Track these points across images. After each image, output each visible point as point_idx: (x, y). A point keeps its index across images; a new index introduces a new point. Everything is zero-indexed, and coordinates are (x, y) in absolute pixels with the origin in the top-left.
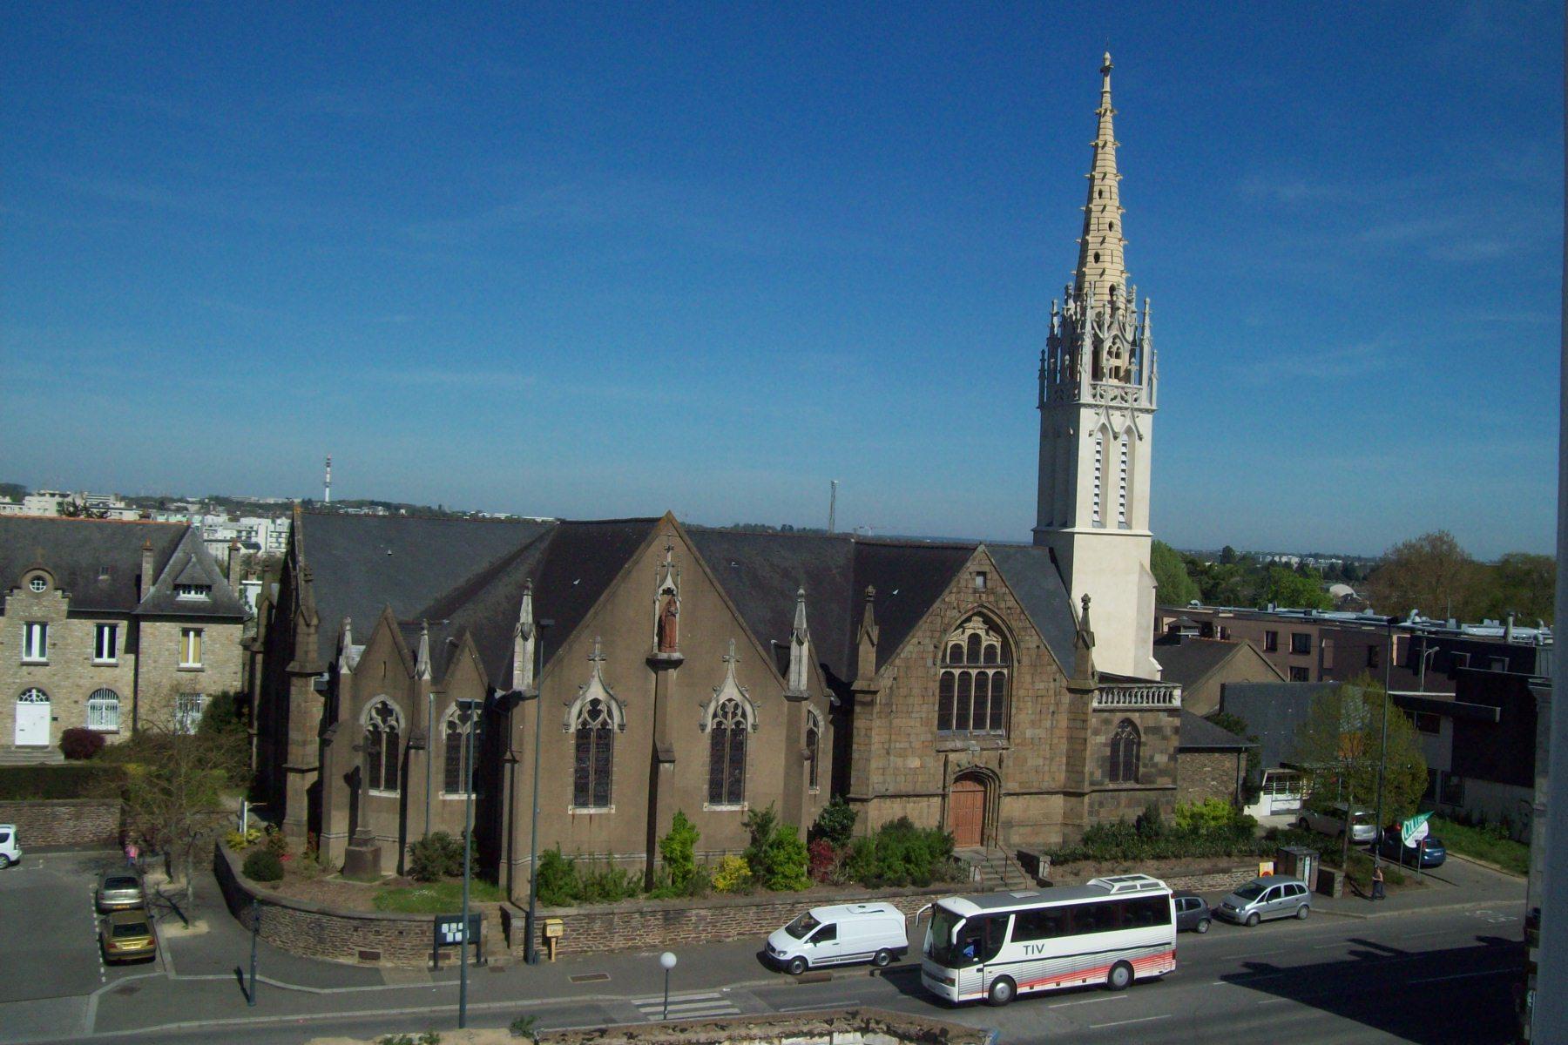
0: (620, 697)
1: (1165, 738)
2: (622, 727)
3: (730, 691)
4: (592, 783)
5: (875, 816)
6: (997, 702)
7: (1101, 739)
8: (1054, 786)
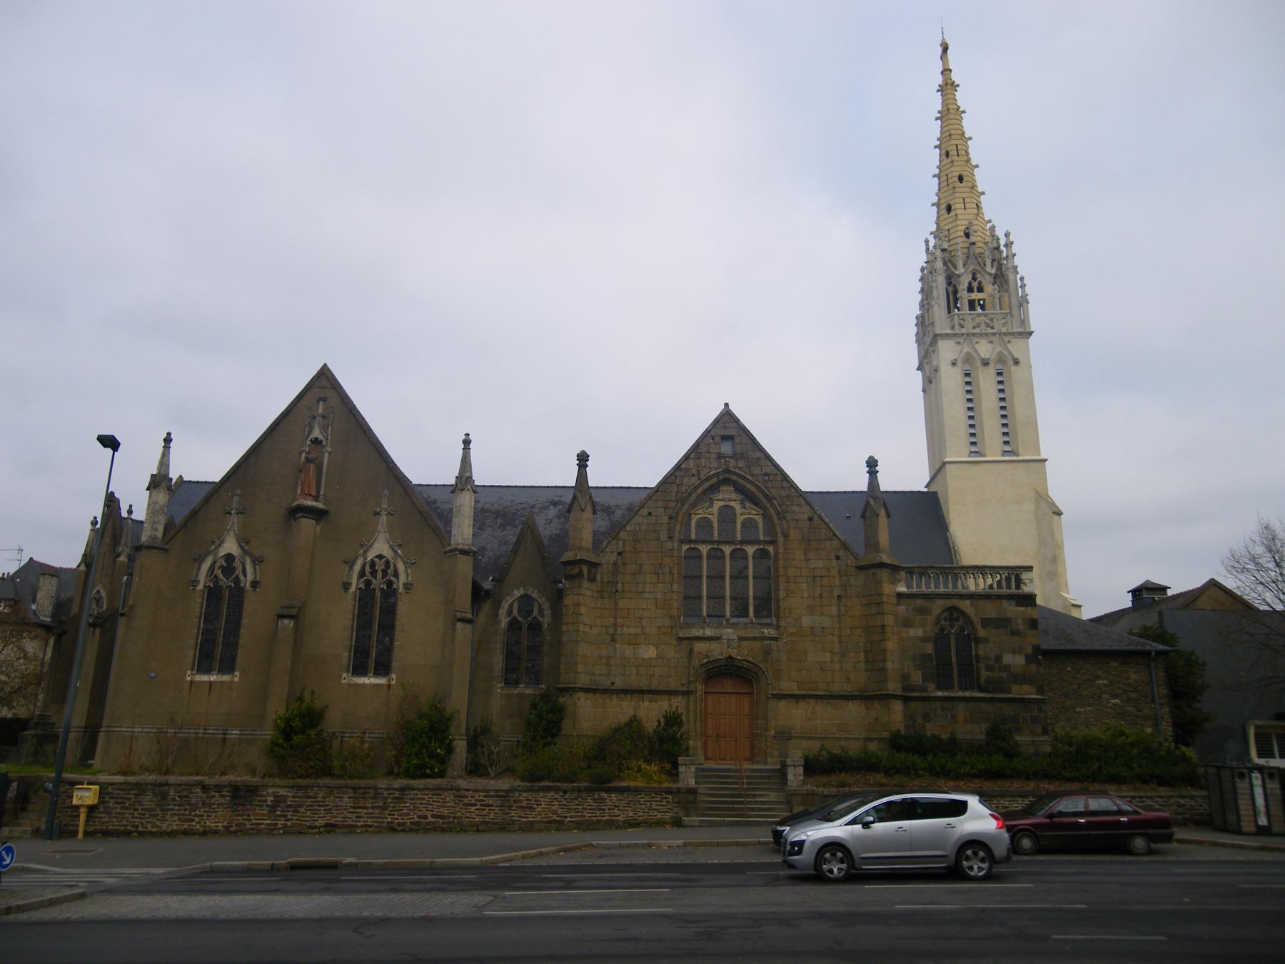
1: (1015, 633)
2: (255, 584)
3: (381, 547)
4: (216, 650)
5: (590, 717)
8: (848, 689)
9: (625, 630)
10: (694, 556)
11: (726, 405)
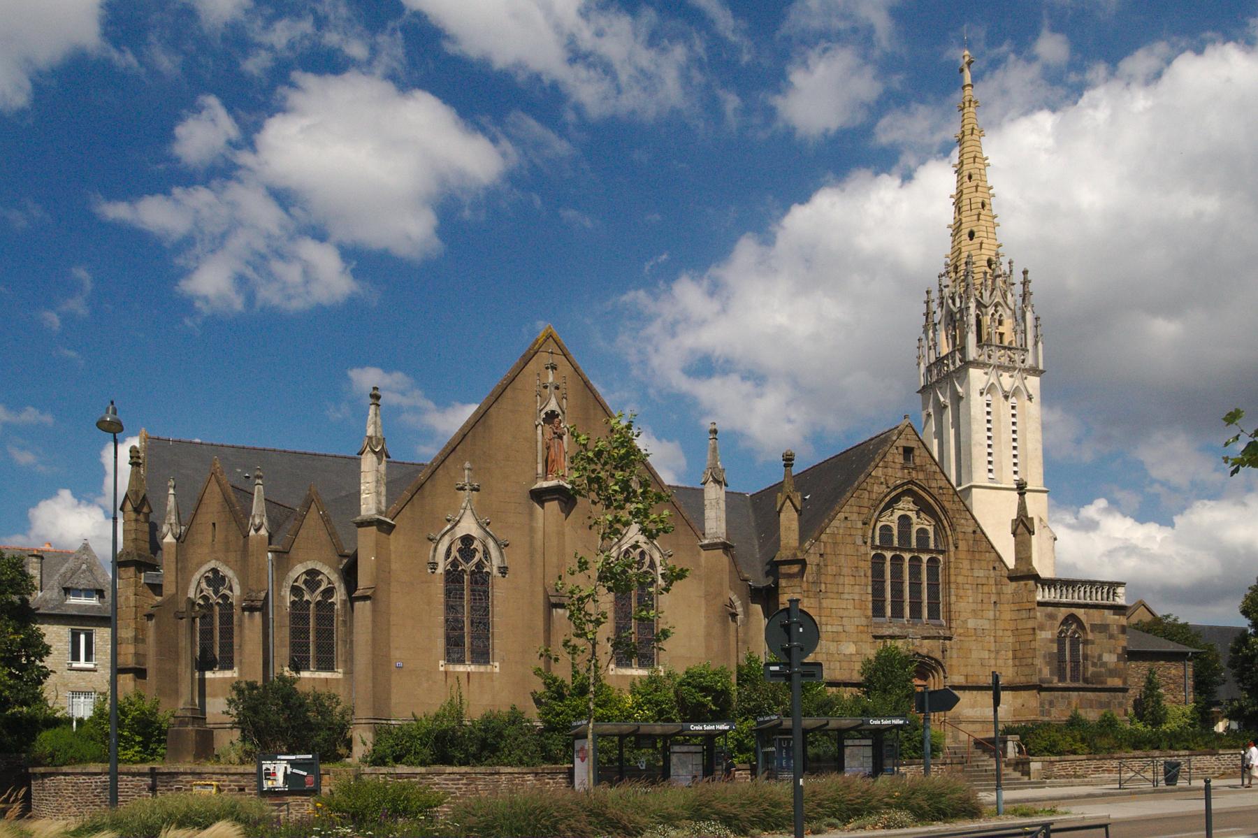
0: (502, 537)
1: (1111, 637)
2: (504, 571)
4: (468, 636)
6: (934, 588)
7: (1046, 635)
9: (829, 628)
10: (879, 559)
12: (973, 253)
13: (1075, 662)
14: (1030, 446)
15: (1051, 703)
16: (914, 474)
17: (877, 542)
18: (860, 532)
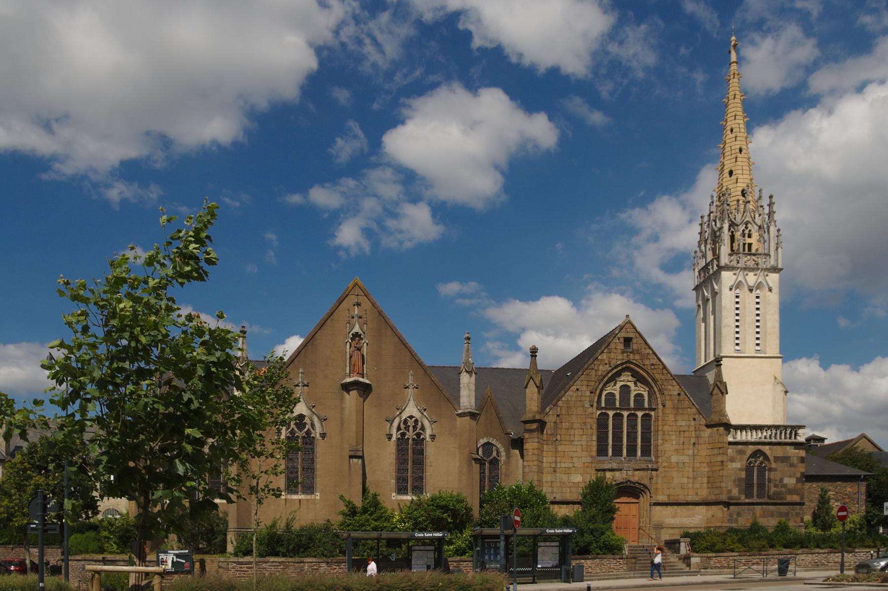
0: (322, 415)
1: (792, 465)
2: (323, 435)
6: (646, 439)
7: (737, 465)
8: (697, 499)
9: (563, 465)
11: (627, 316)
12: (730, 187)
13: (761, 486)
14: (769, 325)
15: (739, 514)
16: (631, 356)
17: (603, 405)
18: (588, 399)
